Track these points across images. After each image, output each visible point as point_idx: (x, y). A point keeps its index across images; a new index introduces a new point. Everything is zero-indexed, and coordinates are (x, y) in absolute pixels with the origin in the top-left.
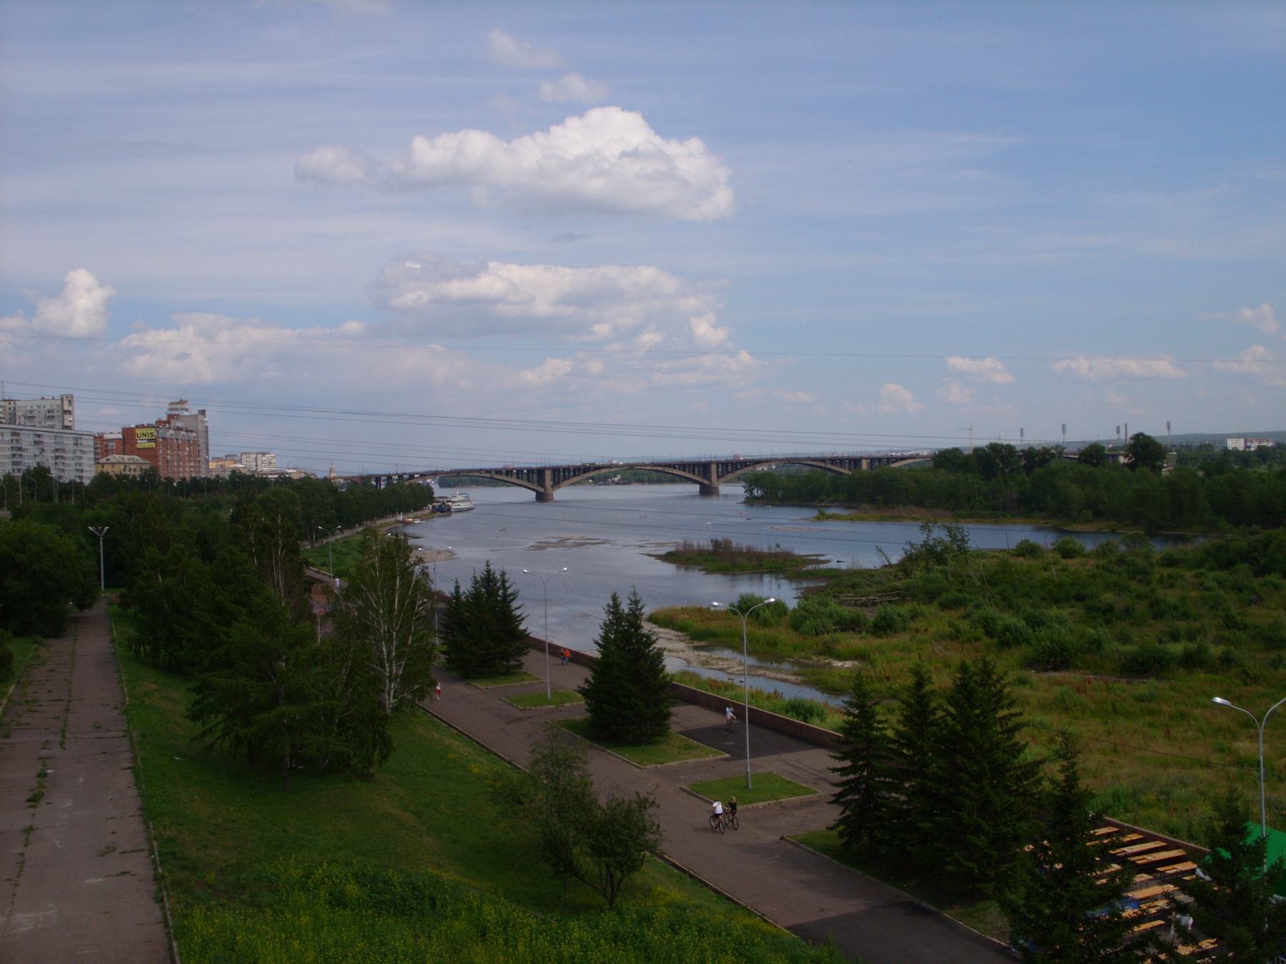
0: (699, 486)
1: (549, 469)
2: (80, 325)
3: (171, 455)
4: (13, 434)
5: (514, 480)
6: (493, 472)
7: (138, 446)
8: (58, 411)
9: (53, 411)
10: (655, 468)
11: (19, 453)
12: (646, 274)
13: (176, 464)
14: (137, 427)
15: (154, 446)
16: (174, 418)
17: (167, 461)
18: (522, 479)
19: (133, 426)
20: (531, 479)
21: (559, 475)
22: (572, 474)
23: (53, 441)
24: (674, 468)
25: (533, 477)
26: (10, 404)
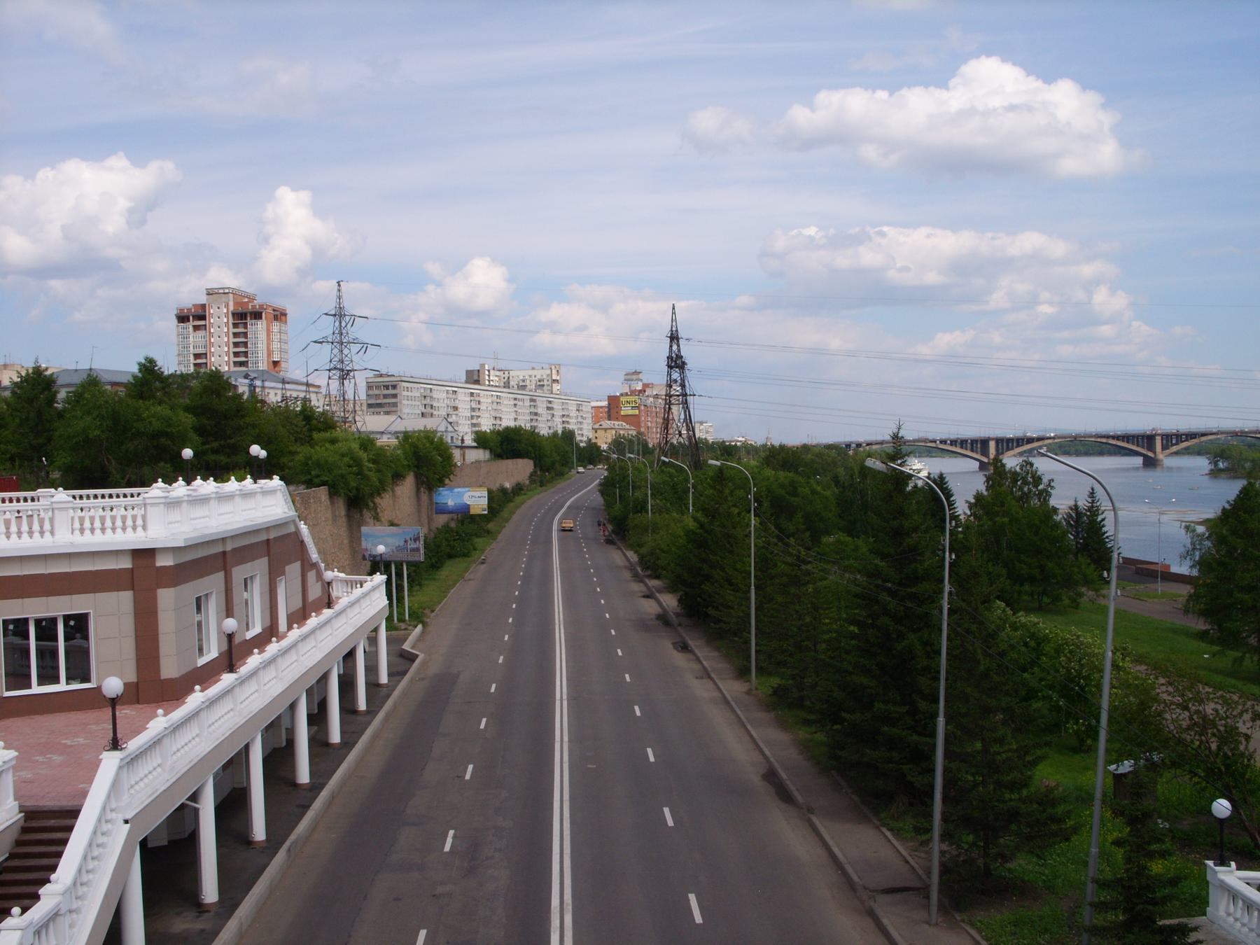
0: (1142, 458)
1: (993, 439)
2: (484, 300)
3: (651, 422)
4: (532, 400)
5: (959, 450)
6: (938, 442)
7: (622, 413)
8: (548, 381)
9: (543, 381)
10: (1099, 440)
11: (535, 417)
12: (1030, 241)
13: (654, 430)
14: (622, 395)
15: (638, 413)
16: (649, 387)
17: (648, 427)
18: (966, 449)
19: (618, 394)
20: (975, 448)
21: (1002, 446)
22: (1015, 444)
23: (419, 403)
24: (1118, 440)
25: (977, 447)
26: (504, 373)
